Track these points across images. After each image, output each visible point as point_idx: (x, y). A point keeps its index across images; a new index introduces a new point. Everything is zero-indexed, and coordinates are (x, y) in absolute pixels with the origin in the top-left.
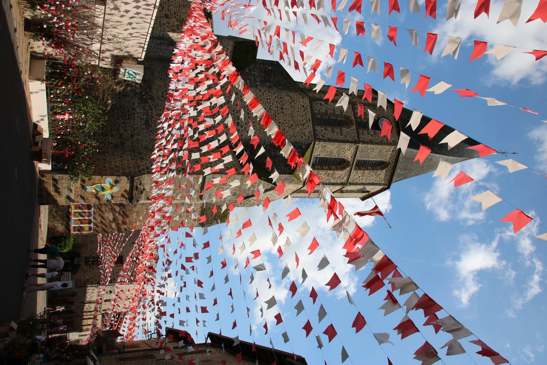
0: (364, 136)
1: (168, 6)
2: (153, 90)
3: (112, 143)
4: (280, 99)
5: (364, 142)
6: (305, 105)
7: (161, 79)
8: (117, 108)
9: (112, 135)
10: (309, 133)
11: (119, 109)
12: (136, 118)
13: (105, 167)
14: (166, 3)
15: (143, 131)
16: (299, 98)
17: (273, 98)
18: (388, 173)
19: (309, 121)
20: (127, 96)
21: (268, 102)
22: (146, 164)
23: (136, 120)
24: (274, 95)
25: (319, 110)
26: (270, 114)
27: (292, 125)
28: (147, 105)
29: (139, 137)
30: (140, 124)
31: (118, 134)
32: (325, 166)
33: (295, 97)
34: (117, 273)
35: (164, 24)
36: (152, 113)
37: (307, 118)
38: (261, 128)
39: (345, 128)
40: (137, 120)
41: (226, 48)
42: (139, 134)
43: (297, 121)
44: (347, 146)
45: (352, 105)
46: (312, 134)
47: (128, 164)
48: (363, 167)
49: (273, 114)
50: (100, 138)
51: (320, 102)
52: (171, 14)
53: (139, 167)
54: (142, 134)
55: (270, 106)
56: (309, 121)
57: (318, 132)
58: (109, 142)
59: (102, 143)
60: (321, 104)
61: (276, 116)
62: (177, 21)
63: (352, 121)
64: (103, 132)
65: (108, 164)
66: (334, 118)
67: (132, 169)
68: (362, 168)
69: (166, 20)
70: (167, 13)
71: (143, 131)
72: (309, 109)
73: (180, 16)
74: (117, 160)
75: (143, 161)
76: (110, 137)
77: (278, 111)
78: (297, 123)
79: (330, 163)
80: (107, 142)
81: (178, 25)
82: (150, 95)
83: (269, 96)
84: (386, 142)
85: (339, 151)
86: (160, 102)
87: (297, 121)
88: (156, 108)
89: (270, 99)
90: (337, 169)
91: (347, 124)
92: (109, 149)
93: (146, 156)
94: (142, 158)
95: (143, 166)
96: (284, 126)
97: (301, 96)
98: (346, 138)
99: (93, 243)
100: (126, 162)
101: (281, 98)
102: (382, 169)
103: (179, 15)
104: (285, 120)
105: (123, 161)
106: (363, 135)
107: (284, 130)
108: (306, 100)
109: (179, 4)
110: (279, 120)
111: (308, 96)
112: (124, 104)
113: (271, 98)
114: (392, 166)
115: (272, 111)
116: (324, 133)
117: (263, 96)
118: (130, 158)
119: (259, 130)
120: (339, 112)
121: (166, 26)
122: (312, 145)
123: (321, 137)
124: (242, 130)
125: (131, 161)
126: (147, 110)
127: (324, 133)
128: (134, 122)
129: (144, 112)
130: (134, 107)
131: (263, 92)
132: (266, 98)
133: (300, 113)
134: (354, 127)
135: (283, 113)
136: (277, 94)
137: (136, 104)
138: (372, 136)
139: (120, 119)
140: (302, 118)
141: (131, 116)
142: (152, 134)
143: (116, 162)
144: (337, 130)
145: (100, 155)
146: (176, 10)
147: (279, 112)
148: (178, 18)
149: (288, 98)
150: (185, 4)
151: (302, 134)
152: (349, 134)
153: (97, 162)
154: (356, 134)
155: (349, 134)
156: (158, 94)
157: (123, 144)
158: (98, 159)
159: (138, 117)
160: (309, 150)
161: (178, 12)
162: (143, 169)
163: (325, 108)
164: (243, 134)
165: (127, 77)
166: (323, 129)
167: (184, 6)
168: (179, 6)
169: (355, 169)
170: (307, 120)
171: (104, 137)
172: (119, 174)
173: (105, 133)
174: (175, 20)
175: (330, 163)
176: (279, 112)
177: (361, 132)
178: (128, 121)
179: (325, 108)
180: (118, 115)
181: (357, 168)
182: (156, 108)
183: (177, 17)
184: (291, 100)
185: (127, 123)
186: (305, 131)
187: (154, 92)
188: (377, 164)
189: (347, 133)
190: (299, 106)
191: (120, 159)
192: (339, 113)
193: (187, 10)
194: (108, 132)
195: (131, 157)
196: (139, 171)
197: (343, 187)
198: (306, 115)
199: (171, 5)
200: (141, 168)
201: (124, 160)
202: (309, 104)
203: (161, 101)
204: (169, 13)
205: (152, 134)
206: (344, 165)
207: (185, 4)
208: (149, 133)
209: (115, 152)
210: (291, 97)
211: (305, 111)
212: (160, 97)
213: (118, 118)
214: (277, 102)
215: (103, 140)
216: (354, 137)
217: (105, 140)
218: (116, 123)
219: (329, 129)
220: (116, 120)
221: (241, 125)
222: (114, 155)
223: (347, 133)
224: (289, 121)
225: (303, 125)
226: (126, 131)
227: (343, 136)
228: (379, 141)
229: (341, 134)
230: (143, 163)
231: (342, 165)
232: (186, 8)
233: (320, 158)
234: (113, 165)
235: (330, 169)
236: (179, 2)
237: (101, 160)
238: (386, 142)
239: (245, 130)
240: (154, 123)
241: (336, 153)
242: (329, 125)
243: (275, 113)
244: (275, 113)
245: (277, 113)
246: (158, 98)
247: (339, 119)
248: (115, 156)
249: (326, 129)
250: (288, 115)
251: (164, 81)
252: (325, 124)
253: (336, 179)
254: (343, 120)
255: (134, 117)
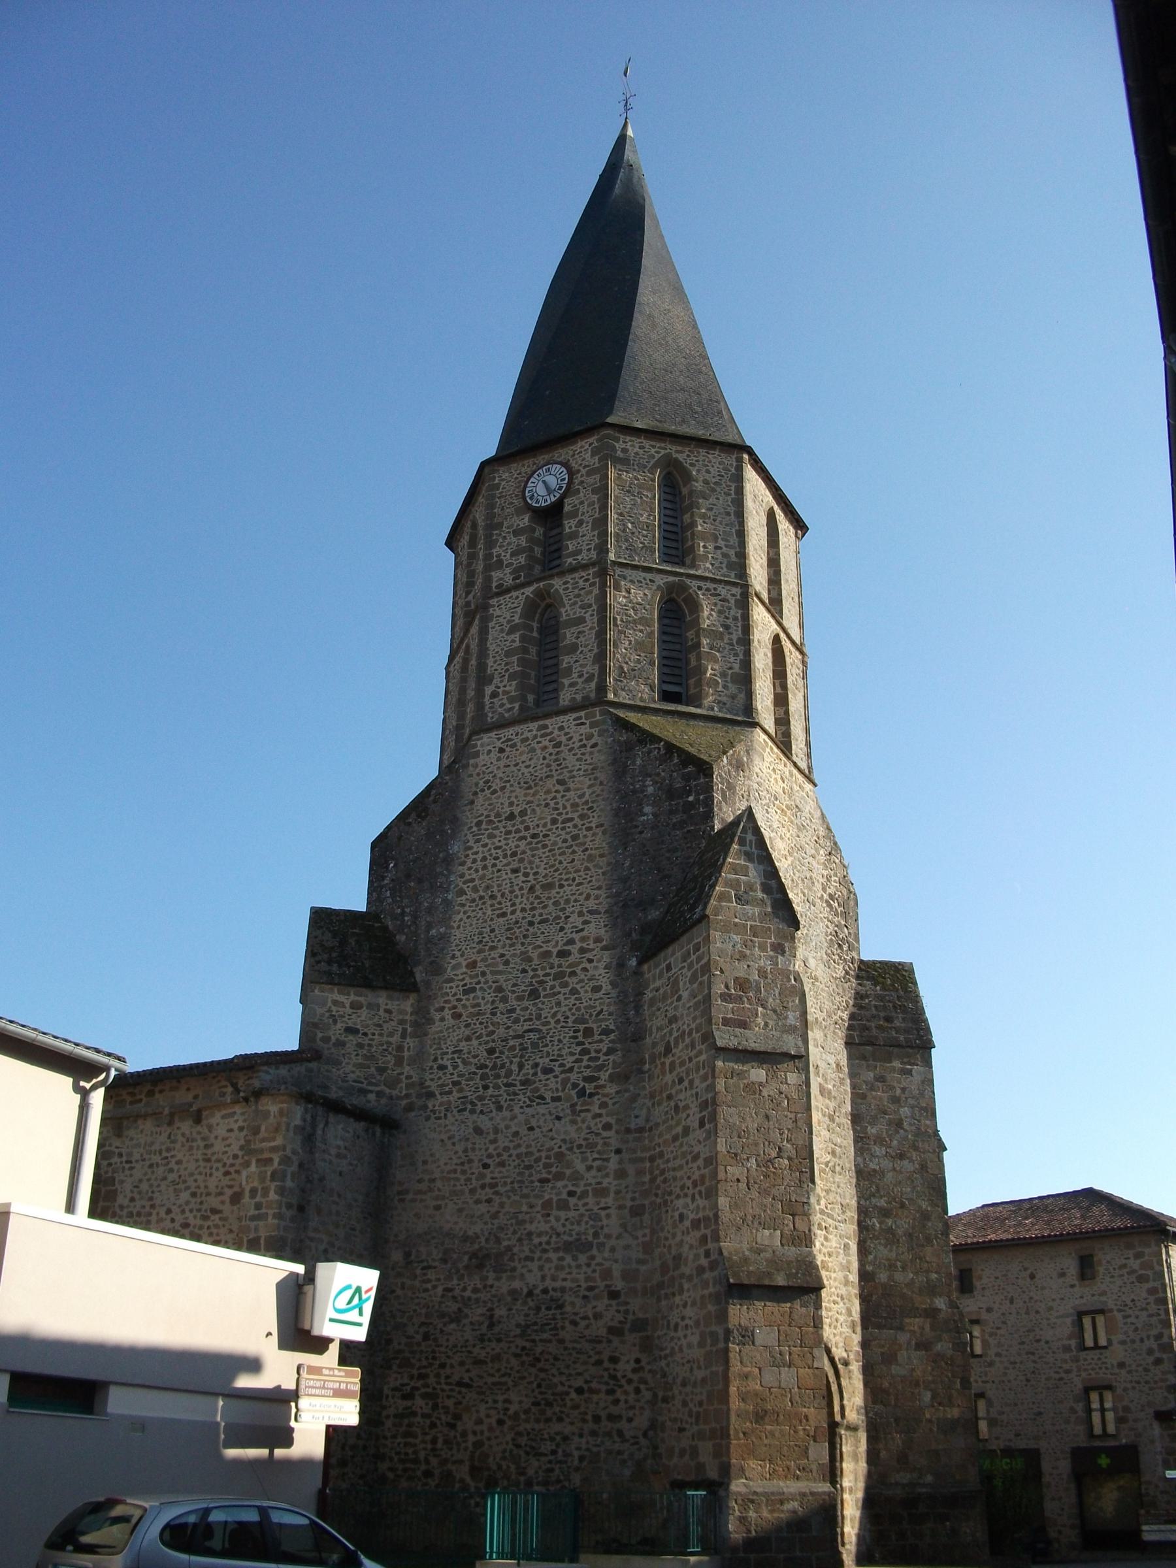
0: (585, 547)
1: (208, 1194)
2: (470, 1233)
3: (638, 1361)
4: (484, 826)
5: (603, 549)
6: (499, 744)
7: (438, 1208)
8: (528, 1345)
9: (614, 1360)
10: (583, 724)
11: (533, 1341)
12: (558, 1284)
13: (704, 1380)
14: (201, 1203)
15: (598, 1260)
16: (476, 766)
17: (481, 849)
18: (701, 458)
19: (546, 727)
20: (492, 1316)
21: (494, 865)
22: (691, 1247)
23: (564, 1284)
24: (470, 848)
25: (512, 700)
26: (529, 852)
27: (561, 782)
28: (515, 1250)
29: (616, 1274)
30: (575, 1271)
31: (609, 1341)
32: (688, 662)
33: (475, 779)
34: (1136, 1329)
35: (258, 1206)
36: (540, 1235)
37: (535, 737)
38: (574, 880)
39: (563, 610)
40: (565, 1280)
41: (334, 1008)
42: (607, 1274)
43: (548, 766)
44: (617, 600)
45: (492, 597)
46: (582, 714)
47: (694, 1304)
48: (684, 541)
49: (531, 843)
50: (623, 1398)
51: (487, 699)
52: (231, 1187)
53: (701, 1270)
54: (607, 1264)
55: (505, 856)
56: (546, 727)
57: (579, 697)
58: (635, 1371)
59: (637, 1391)
60: (494, 695)
61: (534, 836)
62: (247, 1164)
63: (540, 594)
64: (604, 1388)
65: (696, 1372)
66: (533, 650)
67: (706, 1292)
68: (690, 543)
69: (246, 1199)
70: (226, 1198)
71: (598, 1260)
72: (510, 732)
73: (235, 1157)
74: (684, 1342)
75: (684, 1255)
76: (621, 1366)
77: (518, 831)
78: (554, 766)
79: (677, 647)
80: (635, 1377)
81: (258, 1161)
82: (487, 1240)
83: (474, 861)
84: (597, 477)
85: (635, 622)
86: (507, 1208)
87: (548, 766)
88: (524, 1222)
89: (484, 859)
90: (696, 622)
91: (549, 606)
92: (655, 1367)
93: (670, 1246)
94: (678, 1258)
95: (697, 1256)
96: (565, 807)
97: (472, 761)
98: (590, 606)
99: (1040, 1414)
100: (689, 1312)
101: (479, 824)
102: (688, 478)
103: (231, 1161)
104: (547, 805)
105: (687, 1321)
106: (579, 552)
107: (574, 805)
108: (482, 745)
109: (202, 1163)
110: (545, 825)
111: (469, 738)
112: (518, 1325)
113: (480, 856)
114: (674, 448)
115: (519, 850)
116: (580, 676)
117: (477, 882)
118: (677, 1299)
119: (580, 884)
120: (512, 637)
121: (263, 1200)
122: (621, 713)
123: (593, 685)
124: (583, 939)
125: (686, 1294)
126: (532, 1251)
127: (580, 676)
128: (571, 1289)
129: (540, 1259)
130: (525, 1290)
131: (464, 883)
132: (481, 872)
133: (524, 758)
134: (557, 583)
135: (523, 813)
136: (470, 837)
137: (517, 1284)
138: (581, 523)
139: (562, 1334)
140: (539, 751)
141: (552, 1300)
142: (606, 1230)
143: (690, 1346)
144: (568, 635)
145: (673, 1397)
146: (217, 1169)
147: (522, 827)
148: (241, 1164)
149: (480, 800)
150: (202, 1144)
151: (585, 746)
152: (578, 596)
153: (691, 1405)
154: (576, 575)
155: (578, 596)
156: (482, 1215)
157: (639, 1325)
158: (685, 1404)
159: (554, 1279)
160: (633, 717)
161: (224, 1165)
162: (707, 1254)
163: (505, 682)
164: (592, 936)
165: (361, 1314)
166: (566, 682)
167: (206, 1147)
168: (208, 1160)
169: (693, 566)
170: (542, 736)
171: (621, 1386)
172: (720, 1331)
173: (607, 1383)
174: (244, 1174)
175: (677, 647)
176: (522, 827)
177: (570, 560)
178: (568, 1309)
179: (505, 682)
180: (550, 1341)
181: (688, 561)
182: (524, 1222)
183: (237, 1168)
184: (483, 790)
185: (576, 1314)
186: (576, 738)
187: (477, 1228)
188: (675, 495)
189: (575, 603)
190: (502, 763)
191: (680, 1333)
192: (516, 636)
193: (216, 1137)
194: (606, 1374)
195: (674, 1294)
196: (713, 1266)
197: (758, 596)
198: (527, 739)
199: (206, 1187)
200: (704, 1262)
201: (683, 1318)
202: (492, 734)
203: (502, 1205)
204: (229, 1192)
205: (606, 1230)
206: (680, 600)
207: (202, 1144)
208: (602, 1239)
209: (662, 1349)
210: (476, 794)
211: (514, 746)
212: (493, 1210)
213: (561, 1341)
214: (491, 836)
215: (630, 1388)
216: (587, 580)
217: (630, 1381)
218: (574, 1349)
219: (566, 661)
220: (566, 1349)
221: (564, 945)
222: (672, 1353)
223: (575, 603)
224: (548, 792)
225: (558, 745)
226: (597, 1316)
227: (587, 615)
228: (595, 498)
229: (581, 620)
230: (691, 1257)
231: (683, 611)
232: (212, 1140)
233: (662, 682)
234: (697, 1353)
235: (698, 645)
236: (197, 1161)
237: (687, 1395)
238: (597, 477)
239: (582, 930)
240: (572, 1224)
241: (641, 631)
242: (557, 665)
243: (524, 838)
244: (524, 838)
245: (526, 834)
246: (495, 1216)
247: (535, 634)
248: (673, 1348)
249: (569, 671)
250: (529, 798)
251: (443, 1198)
252: (553, 678)
253: (728, 622)
254: (540, 622)
255: (554, 1290)
